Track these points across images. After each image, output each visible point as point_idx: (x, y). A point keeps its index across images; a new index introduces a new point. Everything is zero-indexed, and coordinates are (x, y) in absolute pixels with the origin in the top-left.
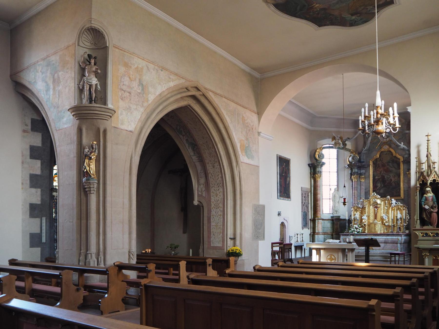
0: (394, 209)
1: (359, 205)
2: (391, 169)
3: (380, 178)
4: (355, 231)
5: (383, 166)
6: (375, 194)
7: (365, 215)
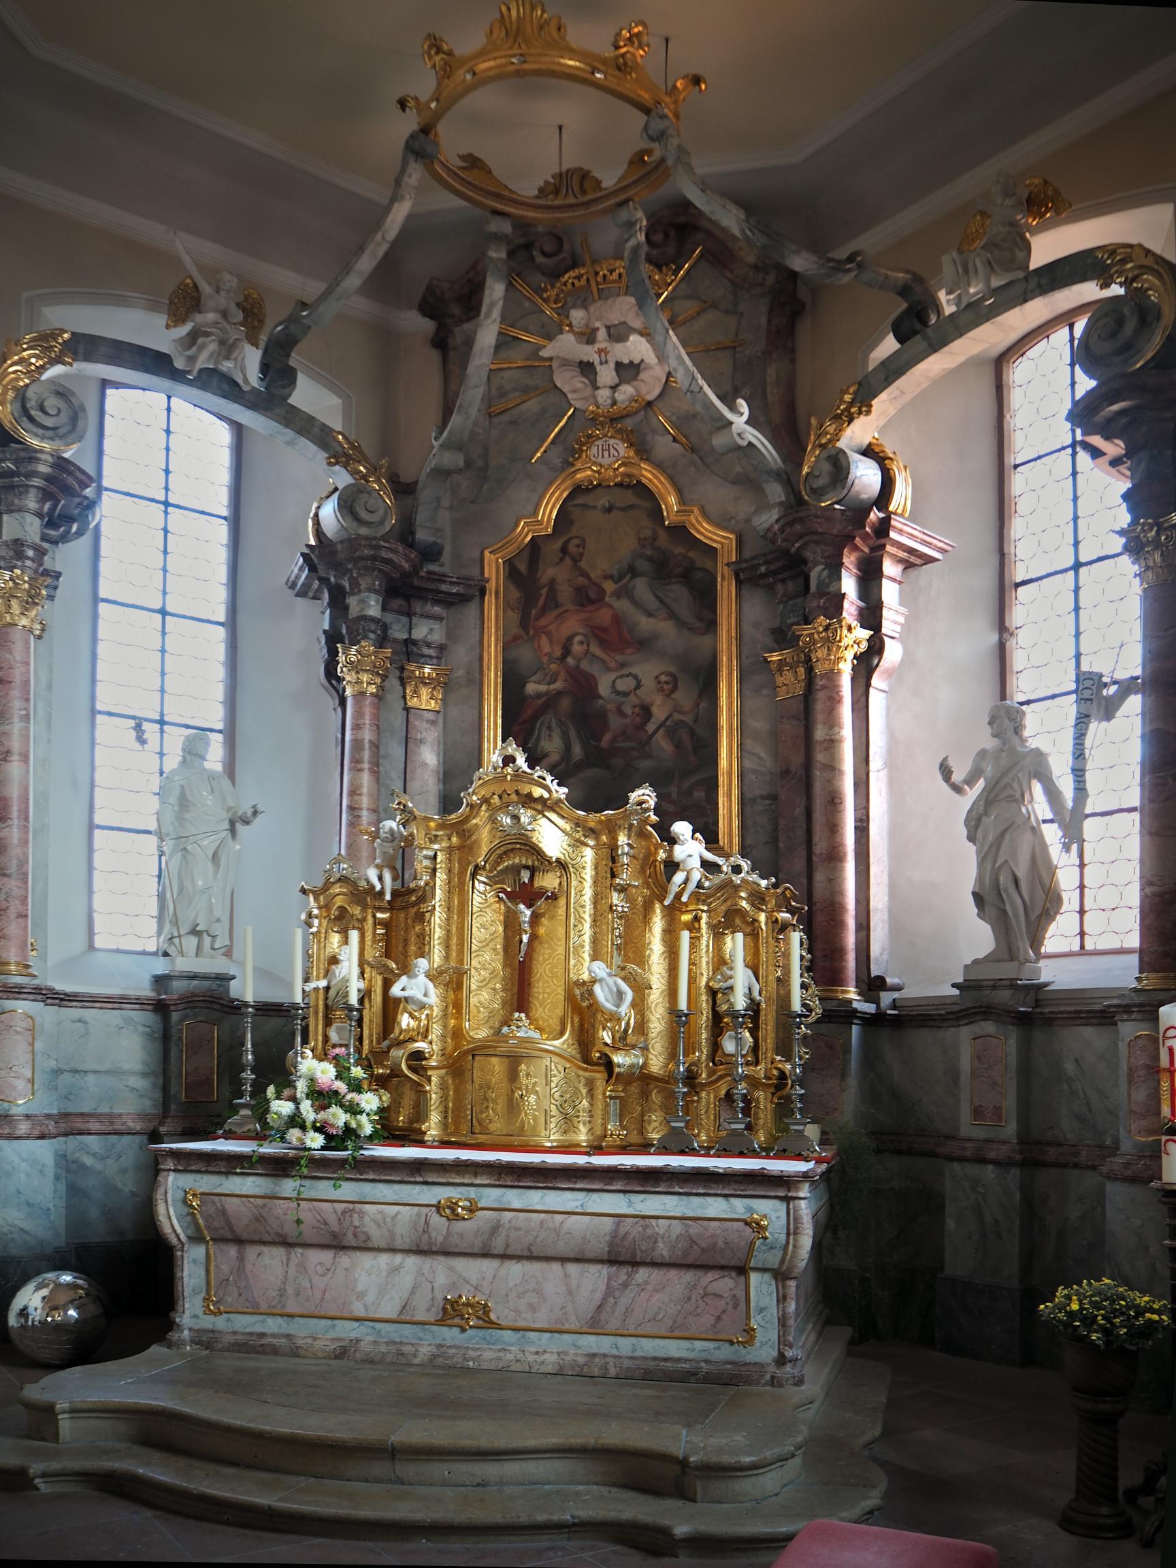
0: (686, 918)
1: (372, 874)
2: (645, 624)
3: (559, 693)
4: (303, 1128)
5: (587, 597)
6: (521, 760)
7: (423, 963)
